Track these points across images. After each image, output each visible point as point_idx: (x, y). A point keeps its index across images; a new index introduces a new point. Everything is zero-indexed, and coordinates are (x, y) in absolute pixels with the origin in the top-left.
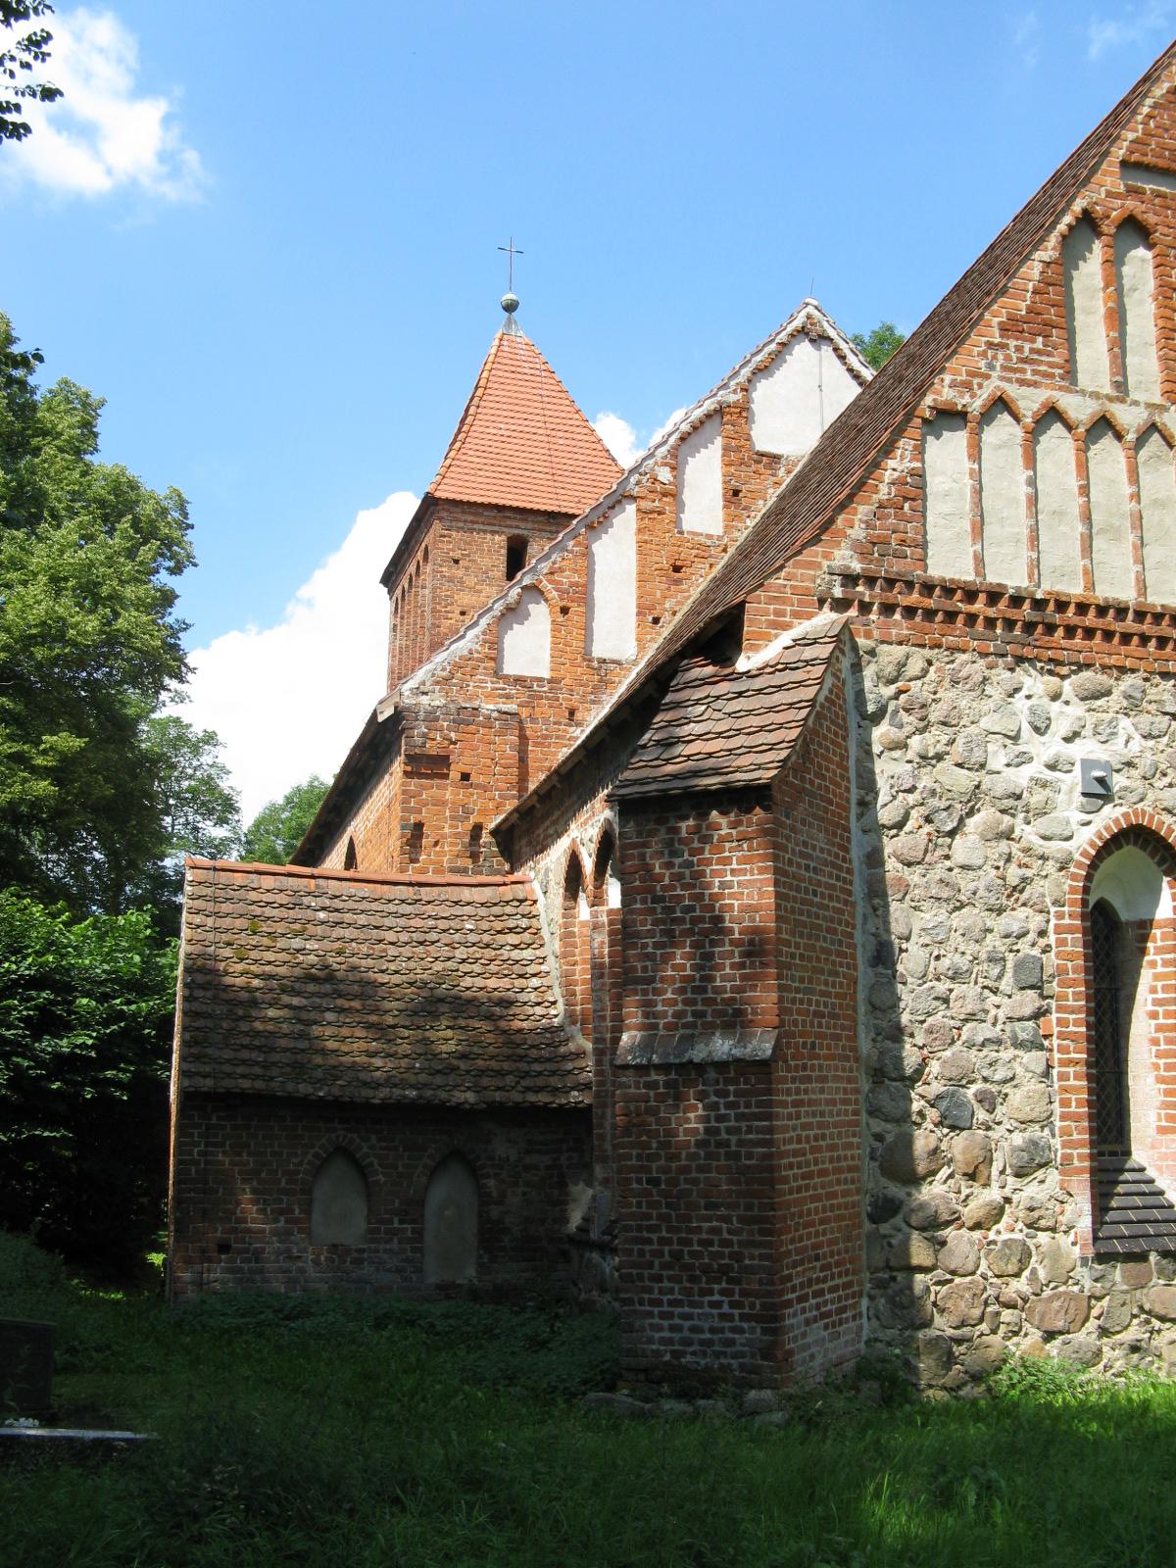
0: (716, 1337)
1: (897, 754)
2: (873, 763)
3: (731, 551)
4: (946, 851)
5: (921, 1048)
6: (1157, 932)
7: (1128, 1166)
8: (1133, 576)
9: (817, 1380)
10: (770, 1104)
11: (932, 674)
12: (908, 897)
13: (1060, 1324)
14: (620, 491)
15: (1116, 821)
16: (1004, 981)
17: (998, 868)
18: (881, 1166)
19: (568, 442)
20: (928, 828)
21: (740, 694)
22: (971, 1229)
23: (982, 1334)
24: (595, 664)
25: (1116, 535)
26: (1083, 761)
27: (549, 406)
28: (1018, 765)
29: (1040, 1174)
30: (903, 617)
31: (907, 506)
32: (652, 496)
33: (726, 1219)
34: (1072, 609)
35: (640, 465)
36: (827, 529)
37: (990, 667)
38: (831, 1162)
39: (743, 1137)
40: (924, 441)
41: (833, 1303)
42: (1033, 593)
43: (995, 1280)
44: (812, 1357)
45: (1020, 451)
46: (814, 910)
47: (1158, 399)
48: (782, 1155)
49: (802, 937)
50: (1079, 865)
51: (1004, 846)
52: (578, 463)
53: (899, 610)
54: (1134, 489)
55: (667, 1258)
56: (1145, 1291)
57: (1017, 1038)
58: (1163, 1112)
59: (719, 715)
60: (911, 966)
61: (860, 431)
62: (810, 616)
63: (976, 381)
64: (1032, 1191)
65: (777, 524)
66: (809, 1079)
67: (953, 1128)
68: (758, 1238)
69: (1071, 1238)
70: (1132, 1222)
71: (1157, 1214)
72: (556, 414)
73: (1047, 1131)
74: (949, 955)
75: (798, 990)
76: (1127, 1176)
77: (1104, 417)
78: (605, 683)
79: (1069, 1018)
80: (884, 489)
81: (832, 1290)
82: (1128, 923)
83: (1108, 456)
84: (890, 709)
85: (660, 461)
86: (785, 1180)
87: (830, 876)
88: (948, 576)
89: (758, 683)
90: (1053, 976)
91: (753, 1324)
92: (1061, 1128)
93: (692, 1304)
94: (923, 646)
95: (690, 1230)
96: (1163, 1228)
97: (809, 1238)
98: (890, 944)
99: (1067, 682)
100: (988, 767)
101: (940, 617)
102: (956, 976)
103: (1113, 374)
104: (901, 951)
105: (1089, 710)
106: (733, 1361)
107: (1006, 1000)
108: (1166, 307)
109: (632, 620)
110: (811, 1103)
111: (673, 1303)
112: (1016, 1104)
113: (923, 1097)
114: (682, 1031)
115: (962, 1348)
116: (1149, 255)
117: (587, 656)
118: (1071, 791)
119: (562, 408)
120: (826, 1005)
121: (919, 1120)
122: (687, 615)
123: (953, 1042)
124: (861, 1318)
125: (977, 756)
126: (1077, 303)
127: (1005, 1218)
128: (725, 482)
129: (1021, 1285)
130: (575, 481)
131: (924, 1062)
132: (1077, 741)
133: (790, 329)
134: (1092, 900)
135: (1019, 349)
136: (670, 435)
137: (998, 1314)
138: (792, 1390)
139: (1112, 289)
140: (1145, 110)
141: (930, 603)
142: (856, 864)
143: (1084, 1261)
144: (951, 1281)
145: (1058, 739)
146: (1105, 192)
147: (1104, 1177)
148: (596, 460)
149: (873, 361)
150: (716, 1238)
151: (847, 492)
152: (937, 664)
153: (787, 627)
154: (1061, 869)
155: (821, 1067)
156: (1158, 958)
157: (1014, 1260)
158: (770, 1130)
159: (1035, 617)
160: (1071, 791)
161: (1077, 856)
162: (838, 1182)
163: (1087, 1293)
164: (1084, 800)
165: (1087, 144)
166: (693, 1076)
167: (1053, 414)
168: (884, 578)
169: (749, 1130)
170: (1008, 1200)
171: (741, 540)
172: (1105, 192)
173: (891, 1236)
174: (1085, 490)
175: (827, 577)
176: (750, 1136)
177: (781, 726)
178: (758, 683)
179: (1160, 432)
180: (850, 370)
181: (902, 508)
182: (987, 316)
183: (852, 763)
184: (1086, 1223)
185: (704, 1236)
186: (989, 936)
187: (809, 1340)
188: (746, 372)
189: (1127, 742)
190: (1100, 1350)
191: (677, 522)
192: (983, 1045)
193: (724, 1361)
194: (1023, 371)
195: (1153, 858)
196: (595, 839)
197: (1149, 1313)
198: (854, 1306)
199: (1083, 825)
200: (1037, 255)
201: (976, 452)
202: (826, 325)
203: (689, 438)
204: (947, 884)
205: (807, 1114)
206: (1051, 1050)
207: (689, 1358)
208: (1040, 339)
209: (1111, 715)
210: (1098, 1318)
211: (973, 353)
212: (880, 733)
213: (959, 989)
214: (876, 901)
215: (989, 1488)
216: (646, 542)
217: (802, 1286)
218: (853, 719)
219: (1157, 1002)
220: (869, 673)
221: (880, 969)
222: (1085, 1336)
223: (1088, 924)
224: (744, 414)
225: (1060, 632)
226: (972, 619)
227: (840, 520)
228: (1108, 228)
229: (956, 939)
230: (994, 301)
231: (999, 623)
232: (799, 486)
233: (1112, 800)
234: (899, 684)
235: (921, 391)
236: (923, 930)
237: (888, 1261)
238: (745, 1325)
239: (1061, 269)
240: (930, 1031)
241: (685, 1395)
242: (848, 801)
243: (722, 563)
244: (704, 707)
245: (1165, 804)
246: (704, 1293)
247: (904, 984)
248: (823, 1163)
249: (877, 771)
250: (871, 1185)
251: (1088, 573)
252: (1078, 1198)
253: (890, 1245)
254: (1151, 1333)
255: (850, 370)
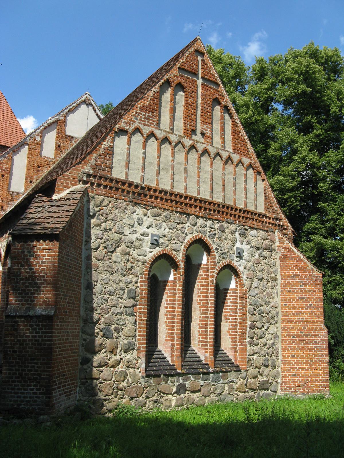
0: (31, 399)
1: (98, 228)
2: (91, 230)
3: (56, 163)
4: (110, 257)
5: (99, 314)
6: (169, 284)
7: (157, 350)
8: (170, 183)
9: (62, 412)
10: (52, 329)
11: (110, 205)
12: (98, 270)
13: (135, 395)
14: (24, 142)
15: (160, 252)
16: (124, 296)
17: (125, 263)
18: (85, 348)
19: (10, 125)
20: (105, 250)
21: (53, 206)
22: (111, 367)
23: (112, 398)
24: (11, 193)
25: (166, 171)
26: (152, 234)
27: (5, 113)
28: (133, 234)
29: (131, 352)
30: (103, 188)
31: (108, 156)
32: (33, 144)
33: (37, 363)
34: (152, 191)
35: (31, 135)
36: (83, 160)
37: (127, 205)
38: (70, 347)
39: (43, 338)
40: (114, 138)
41: (68, 389)
42: (142, 185)
43: (117, 382)
44: (61, 405)
45: (142, 144)
46: (69, 272)
47: (182, 134)
48: (55, 344)
49: (65, 279)
50: (148, 264)
51: (127, 257)
52: (13, 131)
53: (102, 186)
54: (173, 159)
55: (17, 375)
56: (159, 385)
57: (127, 312)
58: (167, 335)
59: (46, 212)
60: (97, 290)
61: (97, 132)
62: (76, 185)
63: (131, 122)
64: (129, 357)
65: (70, 157)
66: (65, 322)
67: (107, 338)
68: (46, 369)
69: (139, 370)
70: (157, 366)
71: (164, 364)
72: (8, 116)
73: (134, 339)
74: (109, 287)
75: (63, 295)
76: (156, 353)
77: (166, 137)
78: (13, 199)
79: (142, 307)
80: (101, 150)
81: (68, 385)
82: (161, 281)
83: (167, 149)
84: (97, 214)
85: (37, 134)
86: (55, 352)
87: (75, 262)
88: (118, 177)
89: (58, 203)
90: (138, 295)
91: (43, 395)
92: (138, 339)
93: (24, 390)
94: (108, 197)
95: (25, 367)
96: (165, 368)
97: (62, 370)
98: (92, 283)
99: (149, 211)
100: (124, 234)
101: (114, 189)
102: (110, 293)
103: (170, 126)
104: (95, 285)
105: (154, 220)
106: (36, 407)
107: (124, 301)
108: (187, 109)
109: (24, 181)
110: (65, 329)
111: (18, 389)
112: (125, 332)
113: (99, 328)
114: (27, 306)
115: (106, 402)
116: (184, 94)
117: (9, 190)
118: (147, 242)
119: (9, 114)
120: (71, 300)
121: (97, 335)
122: (40, 181)
123: (108, 313)
124: (77, 393)
125: (121, 230)
126: (162, 104)
127: (121, 364)
128: (56, 143)
129: (124, 384)
130: (11, 137)
131: (99, 319)
132: (150, 228)
133: (80, 100)
134: (151, 274)
135: (145, 115)
136: (41, 127)
137: (117, 392)
138: (53, 415)
139: (172, 102)
140: (187, 55)
141: (112, 185)
142: (83, 259)
143: (143, 377)
144: (104, 383)
145: (145, 227)
146: (173, 74)
147: (150, 353)
148: (18, 131)
149: (105, 113)
150: (33, 369)
151: (90, 150)
152: (112, 203)
153: (69, 187)
154: (143, 264)
155: (68, 318)
156: (169, 291)
157: (123, 377)
158: (52, 337)
159: (141, 192)
160: (147, 242)
161: (148, 261)
162: (72, 353)
163: (143, 386)
164: (151, 245)
165: (170, 61)
166: (29, 320)
167: (152, 135)
168: (99, 176)
169: (45, 337)
170: (122, 359)
171: (59, 160)
172: (173, 74)
173: (87, 369)
174: (159, 157)
175: (82, 174)
176: (46, 338)
177: (64, 217)
178: (58, 203)
179: (181, 143)
180: (97, 115)
181: (106, 156)
182: (137, 104)
183: (84, 229)
184: (144, 366)
185: (29, 368)
186: (121, 283)
187: (60, 400)
188: (66, 111)
189: (164, 230)
190: (146, 402)
191: (41, 153)
192: (117, 314)
193: (33, 407)
194: (145, 121)
195: (169, 263)
196: (5, 246)
197: (160, 392)
198: (75, 390)
199: (150, 252)
200: (153, 89)
201: (129, 143)
202: (91, 100)
203: (47, 129)
204: (110, 267)
205: (63, 332)
206: (137, 316)
207: (22, 406)
208: (151, 113)
209: (161, 222)
210: (146, 393)
211: (131, 114)
212: (93, 221)
213: (111, 297)
214: (88, 270)
215: (109, 443)
216: (30, 158)
217: (59, 384)
218: (86, 217)
219: (167, 304)
220: (92, 203)
221: (88, 290)
222: (142, 398)
223: (150, 281)
224: (64, 123)
225: (148, 197)
226: (123, 190)
227: (88, 158)
228: (173, 85)
229: (111, 283)
230: (139, 100)
231: (131, 193)
232: (77, 147)
233: (159, 246)
234: (100, 207)
235: (115, 123)
236: (102, 279)
237: (85, 376)
238: (41, 396)
239: (159, 94)
240: (102, 309)
241: (20, 418)
242: (82, 240)
243: (53, 167)
244: (41, 209)
245: (174, 248)
246: (28, 386)
247: (95, 295)
248: (68, 347)
249: (92, 232)
250: (82, 354)
251: (158, 181)
252: (142, 359)
253: (86, 372)
254: (161, 397)
255: (97, 115)
